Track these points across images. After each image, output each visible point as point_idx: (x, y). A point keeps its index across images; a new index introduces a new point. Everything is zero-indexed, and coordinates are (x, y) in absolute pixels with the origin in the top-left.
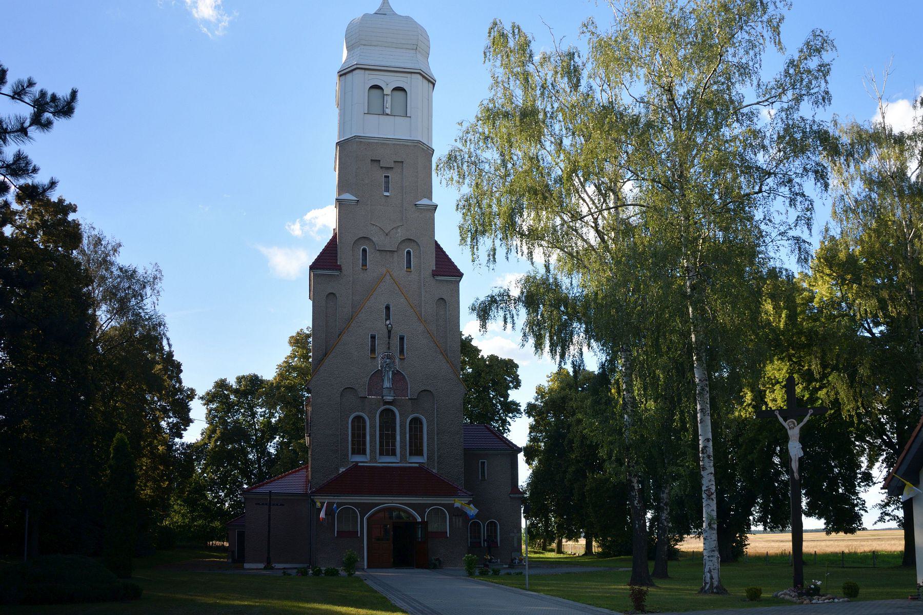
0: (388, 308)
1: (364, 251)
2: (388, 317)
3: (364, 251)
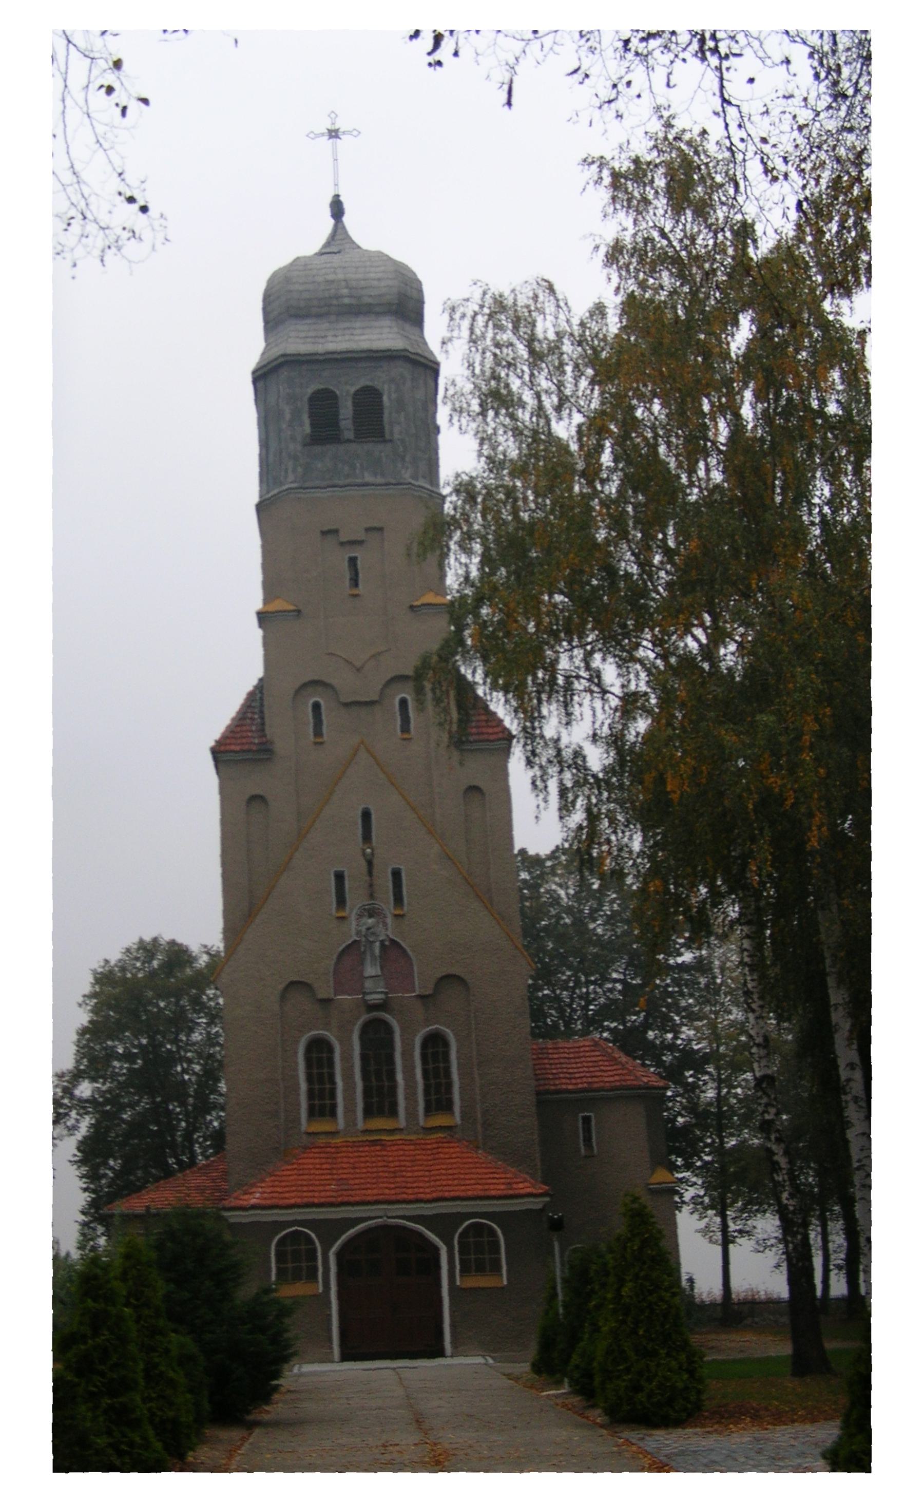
0: (366, 816)
1: (316, 707)
2: (367, 837)
3: (316, 707)
